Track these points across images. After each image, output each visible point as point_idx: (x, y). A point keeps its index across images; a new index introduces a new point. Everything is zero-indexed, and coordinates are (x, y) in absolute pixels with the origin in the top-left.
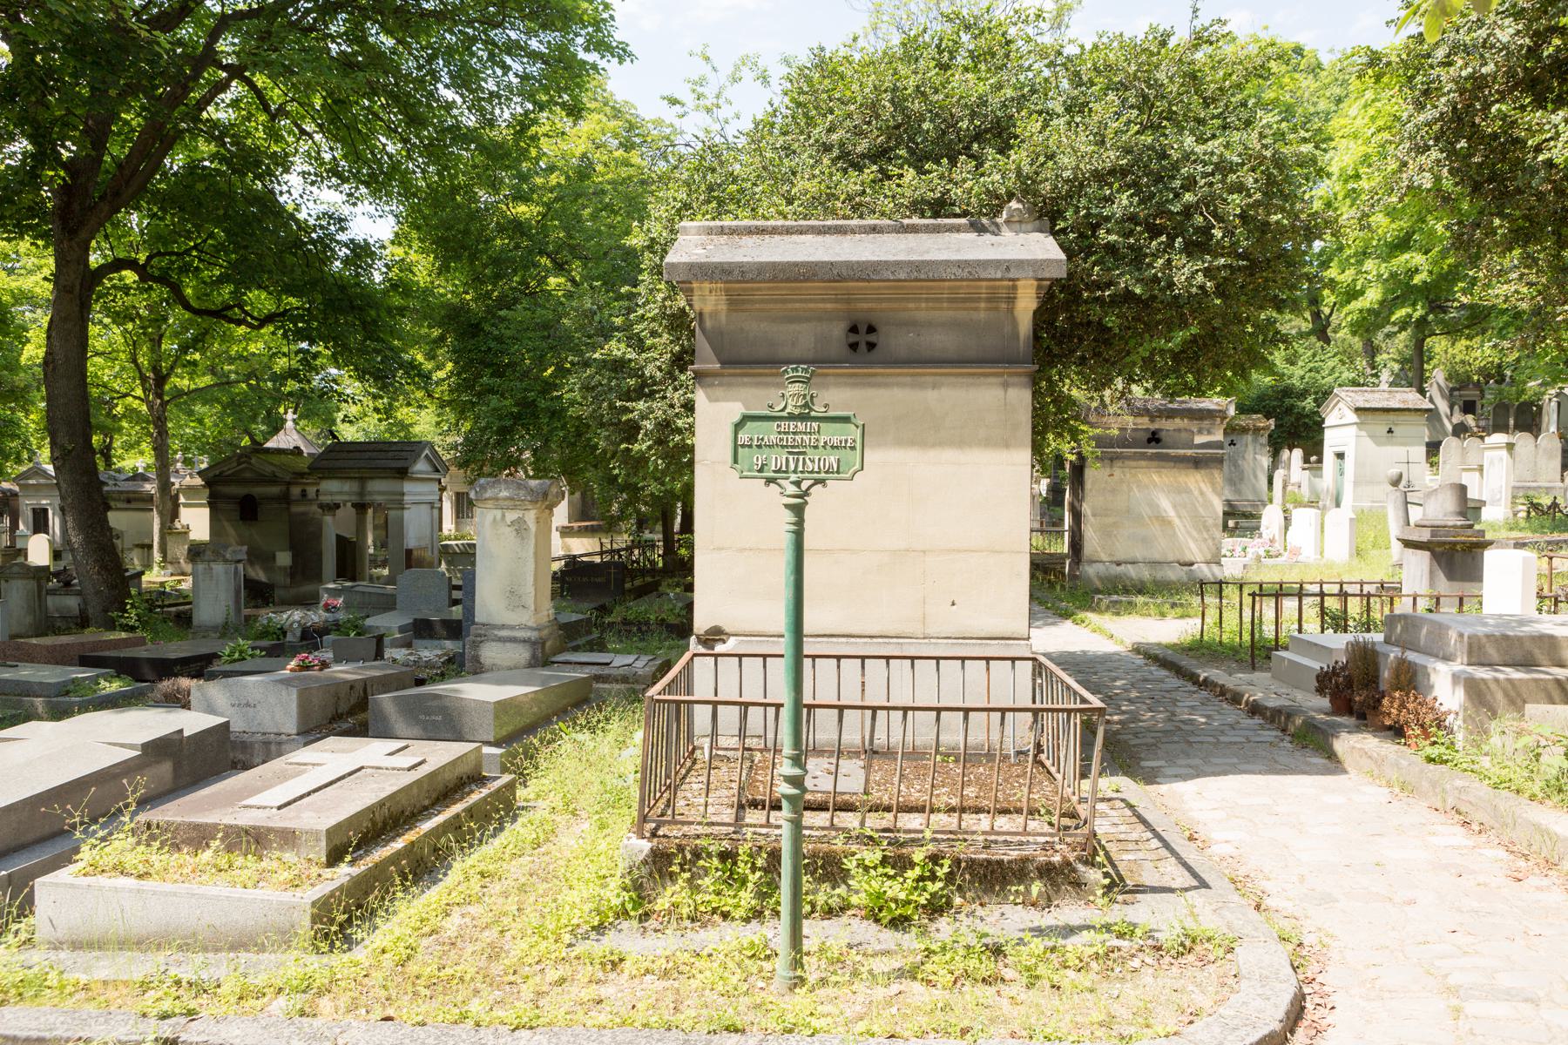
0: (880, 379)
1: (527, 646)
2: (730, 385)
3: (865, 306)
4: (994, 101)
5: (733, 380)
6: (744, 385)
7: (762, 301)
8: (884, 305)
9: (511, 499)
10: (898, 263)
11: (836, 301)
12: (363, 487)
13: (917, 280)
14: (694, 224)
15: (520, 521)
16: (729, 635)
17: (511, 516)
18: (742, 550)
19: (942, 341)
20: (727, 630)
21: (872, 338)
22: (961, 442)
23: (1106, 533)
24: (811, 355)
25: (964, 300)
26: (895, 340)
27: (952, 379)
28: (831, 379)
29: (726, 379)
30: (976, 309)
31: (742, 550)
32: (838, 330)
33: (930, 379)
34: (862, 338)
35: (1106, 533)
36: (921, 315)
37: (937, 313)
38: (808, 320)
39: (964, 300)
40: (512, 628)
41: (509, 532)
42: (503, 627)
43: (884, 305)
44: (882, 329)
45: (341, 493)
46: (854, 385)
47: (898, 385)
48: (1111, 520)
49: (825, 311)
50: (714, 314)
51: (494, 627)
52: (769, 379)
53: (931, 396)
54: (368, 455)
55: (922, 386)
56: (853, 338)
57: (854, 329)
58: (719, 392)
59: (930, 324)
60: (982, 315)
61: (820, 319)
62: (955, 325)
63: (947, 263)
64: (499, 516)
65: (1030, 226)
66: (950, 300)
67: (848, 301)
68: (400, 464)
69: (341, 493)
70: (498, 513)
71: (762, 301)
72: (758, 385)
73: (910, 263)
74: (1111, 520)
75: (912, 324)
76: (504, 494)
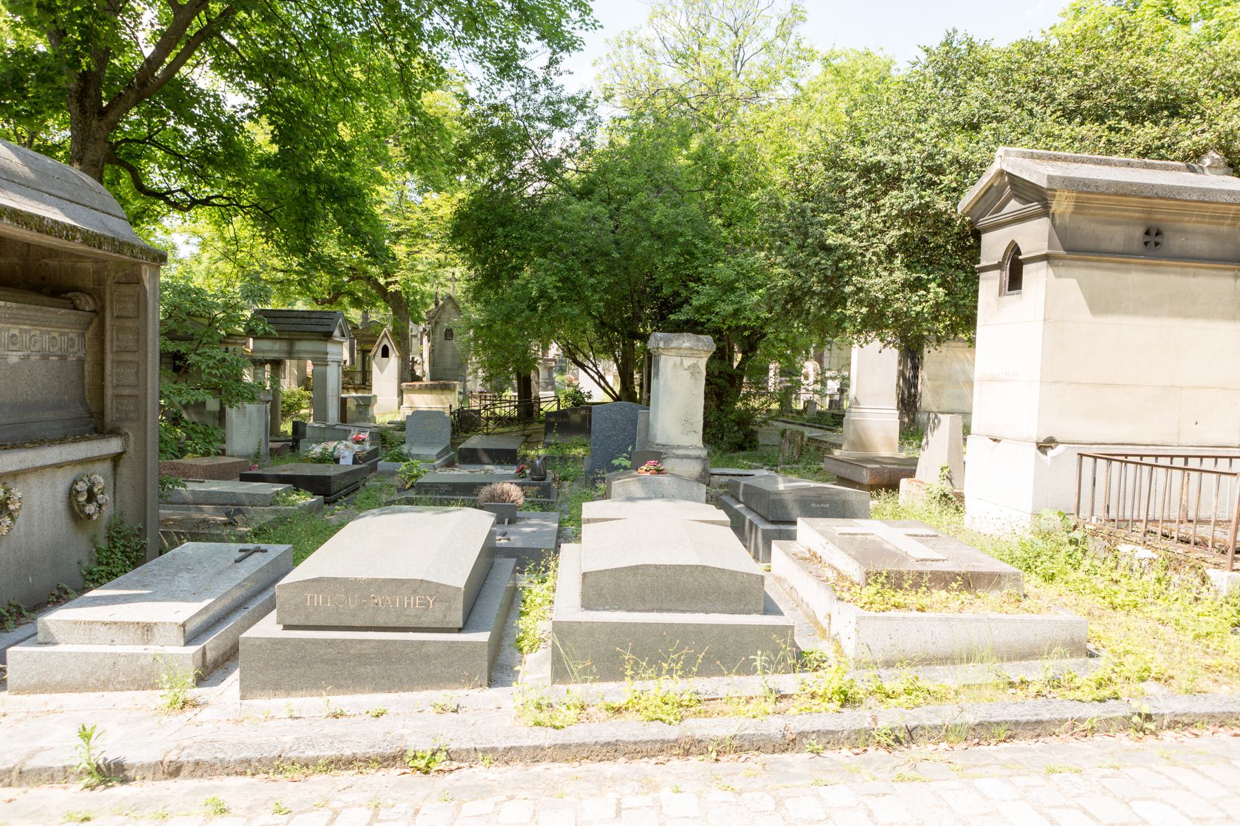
0: (1161, 268)
1: (700, 462)
2: (1069, 266)
3: (1158, 216)
4: (518, 109)
5: (1072, 263)
6: (1078, 266)
7: (1097, 208)
8: (1171, 217)
9: (691, 349)
10: (1192, 189)
11: (1142, 212)
12: (291, 346)
13: (1203, 202)
14: (1014, 149)
15: (695, 366)
16: (1058, 443)
17: (688, 362)
18: (1070, 383)
19: (1200, 245)
20: (1058, 439)
21: (1158, 239)
22: (1208, 315)
23: (936, 392)
24: (1120, 249)
25: (1219, 218)
26: (1174, 242)
27: (1204, 271)
28: (1132, 266)
29: (1066, 262)
30: (1222, 224)
31: (1070, 383)
32: (1139, 232)
33: (1192, 270)
34: (1152, 239)
35: (936, 392)
36: (1189, 226)
37: (1199, 225)
38: (1121, 224)
39: (1219, 218)
40: (686, 448)
41: (686, 375)
42: (679, 447)
43: (1171, 217)
44: (1166, 234)
45: (271, 351)
46: (1147, 271)
47: (1174, 273)
48: (939, 383)
49: (1132, 218)
50: (1062, 215)
51: (673, 447)
52: (1095, 264)
53: (1192, 281)
54: (294, 321)
55: (1187, 275)
56: (1147, 239)
57: (1147, 233)
58: (1062, 270)
59: (1194, 232)
60: (1225, 228)
61: (1128, 224)
62: (1209, 234)
63: (1221, 191)
64: (678, 362)
65: (1221, 171)
66: (1211, 217)
67: (1149, 212)
68: (325, 329)
69: (271, 351)
70: (678, 359)
71: (1097, 208)
72: (1087, 267)
73: (1200, 189)
74: (939, 383)
75: (1183, 232)
76: (687, 344)
